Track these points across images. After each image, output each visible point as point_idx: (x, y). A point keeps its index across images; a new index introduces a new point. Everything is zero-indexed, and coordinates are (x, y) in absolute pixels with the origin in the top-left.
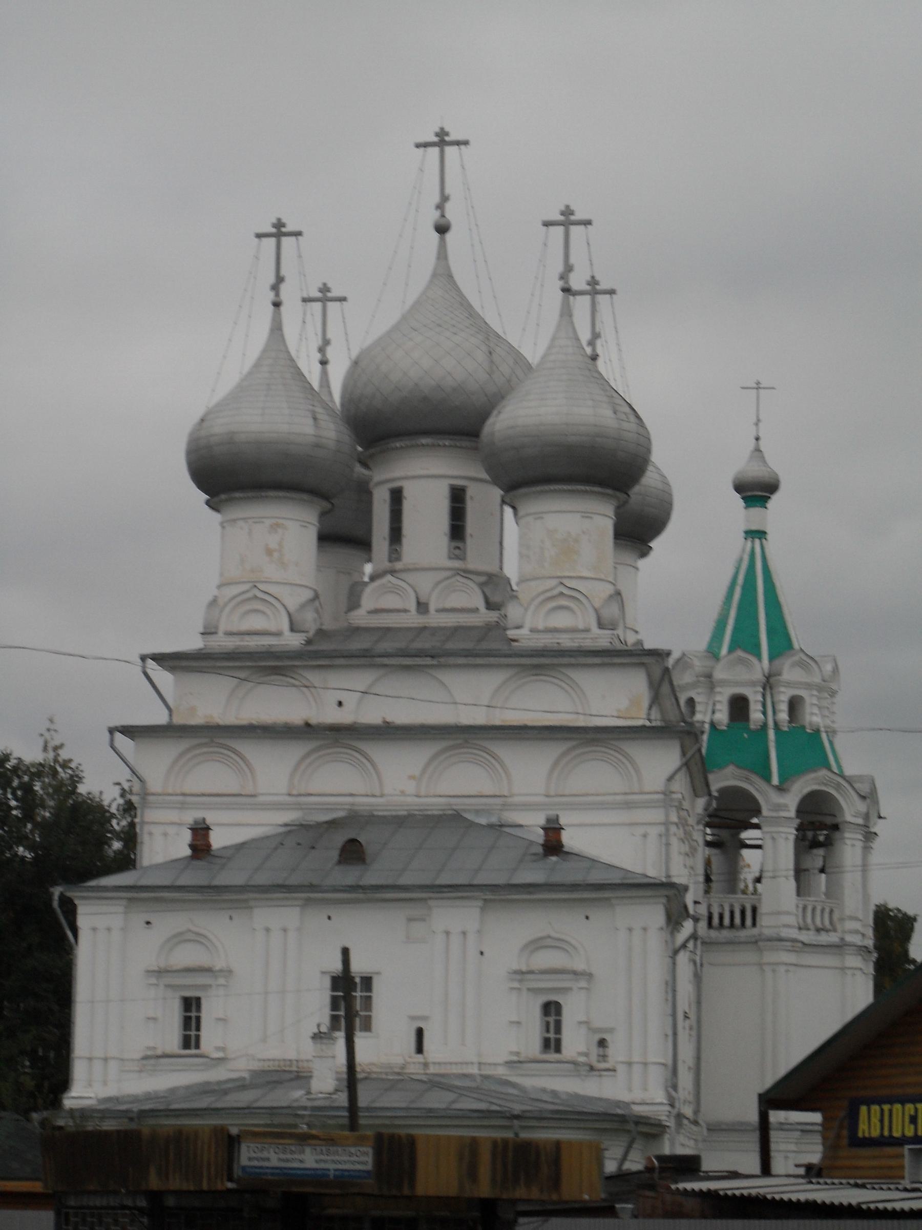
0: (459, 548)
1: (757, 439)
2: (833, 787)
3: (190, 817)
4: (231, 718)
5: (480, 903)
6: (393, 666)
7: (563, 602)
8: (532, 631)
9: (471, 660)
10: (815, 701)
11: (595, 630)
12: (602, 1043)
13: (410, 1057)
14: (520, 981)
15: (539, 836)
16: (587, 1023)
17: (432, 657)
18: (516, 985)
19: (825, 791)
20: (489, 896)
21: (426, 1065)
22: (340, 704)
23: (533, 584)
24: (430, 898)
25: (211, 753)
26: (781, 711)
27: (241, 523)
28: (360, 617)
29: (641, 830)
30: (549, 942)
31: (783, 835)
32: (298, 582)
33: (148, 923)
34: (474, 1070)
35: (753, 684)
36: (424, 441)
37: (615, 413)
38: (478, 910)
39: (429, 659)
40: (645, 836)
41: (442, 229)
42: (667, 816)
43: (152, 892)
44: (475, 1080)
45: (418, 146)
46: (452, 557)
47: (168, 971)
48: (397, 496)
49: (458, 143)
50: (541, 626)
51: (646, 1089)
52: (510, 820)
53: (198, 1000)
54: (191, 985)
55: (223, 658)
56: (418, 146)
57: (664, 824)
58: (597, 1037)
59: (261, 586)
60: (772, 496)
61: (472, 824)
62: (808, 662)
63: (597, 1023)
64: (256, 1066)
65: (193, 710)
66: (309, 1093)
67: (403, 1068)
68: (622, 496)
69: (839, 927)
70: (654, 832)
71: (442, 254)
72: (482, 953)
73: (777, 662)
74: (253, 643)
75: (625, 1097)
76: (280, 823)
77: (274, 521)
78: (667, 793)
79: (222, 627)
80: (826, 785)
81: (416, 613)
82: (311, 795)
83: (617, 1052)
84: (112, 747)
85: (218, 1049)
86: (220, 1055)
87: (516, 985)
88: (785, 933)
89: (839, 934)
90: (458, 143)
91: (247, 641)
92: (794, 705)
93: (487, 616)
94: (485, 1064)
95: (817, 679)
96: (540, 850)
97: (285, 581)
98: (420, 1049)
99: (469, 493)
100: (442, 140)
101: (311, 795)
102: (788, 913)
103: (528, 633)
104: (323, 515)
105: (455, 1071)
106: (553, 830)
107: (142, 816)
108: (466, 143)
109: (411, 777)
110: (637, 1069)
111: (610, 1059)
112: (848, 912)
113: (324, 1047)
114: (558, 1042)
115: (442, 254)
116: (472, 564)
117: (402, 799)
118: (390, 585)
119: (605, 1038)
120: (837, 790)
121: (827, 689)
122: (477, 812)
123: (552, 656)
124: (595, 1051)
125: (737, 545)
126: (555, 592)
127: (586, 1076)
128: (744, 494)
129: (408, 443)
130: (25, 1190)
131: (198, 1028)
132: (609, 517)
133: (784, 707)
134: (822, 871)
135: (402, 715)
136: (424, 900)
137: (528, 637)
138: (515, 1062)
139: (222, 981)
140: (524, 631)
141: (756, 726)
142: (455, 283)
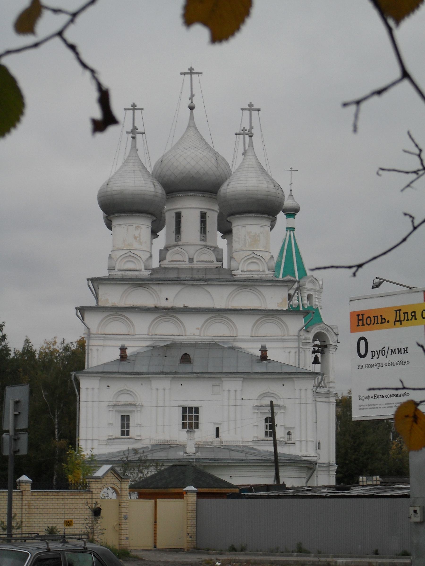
0: (204, 237)
1: (291, 191)
2: (325, 331)
3: (120, 343)
4: (122, 304)
5: (242, 379)
6: (188, 284)
11: (267, 271)
12: (289, 433)
13: (214, 439)
14: (258, 409)
15: (259, 354)
17: (205, 281)
18: (256, 411)
19: (325, 334)
20: (246, 377)
21: (221, 442)
22: (167, 299)
23: (241, 253)
25: (116, 318)
26: (304, 300)
27: (123, 226)
28: (165, 264)
29: (288, 350)
31: (308, 350)
32: (146, 250)
33: (108, 386)
34: (240, 444)
36: (191, 194)
37: (274, 186)
38: (241, 382)
39: (204, 282)
40: (289, 352)
41: (192, 108)
42: (299, 345)
43: (88, 374)
44: (241, 448)
45: (182, 74)
46: (202, 240)
47: (117, 405)
48: (178, 216)
49: (198, 73)
50: (245, 270)
51: (307, 451)
52: (236, 346)
54: (126, 411)
55: (119, 280)
56: (182, 74)
58: (287, 431)
60: (297, 214)
63: (288, 426)
64: (153, 442)
65: (107, 300)
66: (186, 453)
67: (212, 443)
68: (273, 218)
69: (327, 386)
70: (293, 351)
75: (299, 454)
76: (145, 346)
77: (137, 225)
78: (298, 336)
79: (117, 267)
80: (323, 330)
81: (188, 263)
82: (157, 335)
83: (295, 436)
84: (76, 315)
85: (138, 436)
86: (139, 438)
87: (256, 411)
89: (327, 389)
90: (198, 73)
91: (127, 273)
92: (309, 297)
93: (217, 264)
94: (244, 441)
96: (260, 358)
97: (142, 250)
98: (217, 435)
99: (207, 215)
100: (191, 72)
101: (157, 335)
103: (240, 272)
104: (153, 222)
105: (233, 444)
106: (264, 350)
107: (89, 343)
109: (198, 329)
110: (304, 443)
111: (292, 440)
112: (331, 380)
113: (191, 435)
116: (209, 243)
117: (194, 337)
118: (177, 251)
119: (290, 431)
120: (327, 332)
121: (320, 291)
122: (224, 342)
123: (253, 282)
124: (287, 436)
126: (251, 256)
127: (284, 446)
128: (286, 213)
129: (185, 194)
130: (206, 491)
132: (269, 226)
135: (191, 304)
136: (220, 378)
137: (240, 274)
139: (139, 409)
140: (239, 271)
141: (295, 306)
142: (198, 130)
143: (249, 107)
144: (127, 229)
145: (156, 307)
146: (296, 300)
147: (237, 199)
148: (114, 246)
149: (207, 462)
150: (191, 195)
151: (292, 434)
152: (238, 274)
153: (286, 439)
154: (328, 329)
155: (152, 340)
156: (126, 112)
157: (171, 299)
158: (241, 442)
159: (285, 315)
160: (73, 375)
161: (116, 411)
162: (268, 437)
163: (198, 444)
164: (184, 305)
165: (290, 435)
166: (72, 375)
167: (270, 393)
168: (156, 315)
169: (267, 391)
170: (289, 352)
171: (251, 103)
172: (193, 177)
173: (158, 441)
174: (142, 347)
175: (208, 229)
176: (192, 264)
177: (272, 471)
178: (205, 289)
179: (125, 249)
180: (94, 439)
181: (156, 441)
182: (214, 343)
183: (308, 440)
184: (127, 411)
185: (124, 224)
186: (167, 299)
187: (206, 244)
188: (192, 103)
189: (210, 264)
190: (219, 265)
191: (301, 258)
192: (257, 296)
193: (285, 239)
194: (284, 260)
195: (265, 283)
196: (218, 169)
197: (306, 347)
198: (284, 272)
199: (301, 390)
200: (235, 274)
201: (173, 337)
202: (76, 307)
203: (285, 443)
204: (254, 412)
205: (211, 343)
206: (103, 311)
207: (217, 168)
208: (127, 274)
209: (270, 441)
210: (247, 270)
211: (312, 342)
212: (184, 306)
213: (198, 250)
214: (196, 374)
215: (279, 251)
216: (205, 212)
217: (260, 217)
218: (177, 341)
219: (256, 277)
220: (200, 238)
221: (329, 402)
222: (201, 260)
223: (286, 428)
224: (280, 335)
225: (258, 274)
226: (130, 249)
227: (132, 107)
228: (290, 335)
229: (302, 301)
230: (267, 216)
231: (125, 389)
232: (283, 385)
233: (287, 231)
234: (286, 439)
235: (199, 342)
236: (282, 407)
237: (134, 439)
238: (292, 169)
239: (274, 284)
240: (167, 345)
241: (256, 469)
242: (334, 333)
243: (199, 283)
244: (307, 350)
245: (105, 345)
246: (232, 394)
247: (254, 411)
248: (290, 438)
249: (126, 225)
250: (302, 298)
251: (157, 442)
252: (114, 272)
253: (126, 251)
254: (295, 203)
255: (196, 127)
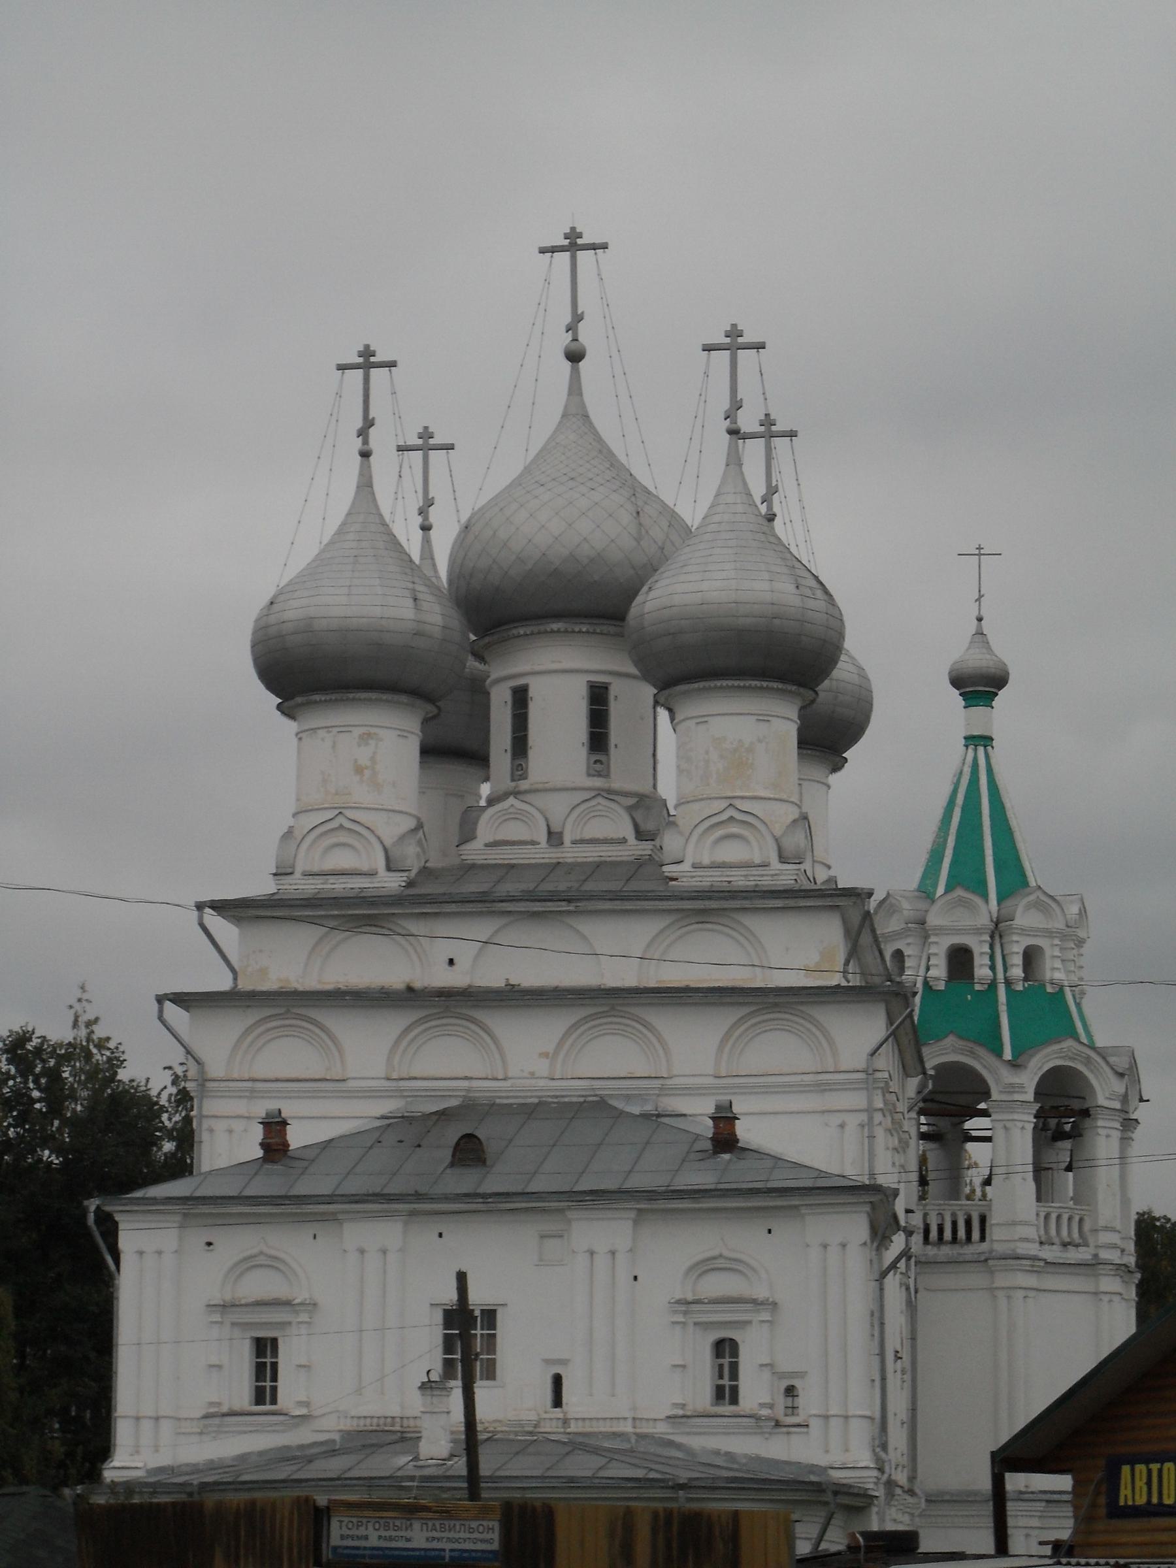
1: (980, 619)
2: (1081, 1062)
3: (261, 1108)
4: (311, 983)
5: (633, 1215)
7: (734, 829)
8: (694, 866)
9: (617, 905)
10: (1057, 953)
12: (790, 1391)
14: (685, 1313)
15: (706, 1128)
16: (770, 1366)
17: (569, 901)
21: (566, 1422)
22: (451, 962)
24: (569, 1208)
27: (321, 733)
28: (475, 851)
29: (836, 1120)
30: (720, 1263)
31: (1020, 1124)
33: (209, 1244)
34: (628, 1428)
35: (978, 931)
36: (555, 626)
38: (630, 1223)
39: (564, 903)
40: (842, 1126)
41: (575, 356)
42: (870, 1101)
44: (629, 1441)
45: (543, 251)
48: (521, 697)
49: (594, 247)
50: (706, 861)
53: (274, 1341)
54: (265, 1322)
56: (543, 251)
57: (866, 1110)
59: (348, 813)
61: (621, 1114)
62: (1047, 903)
63: (785, 1366)
64: (348, 1425)
65: (263, 971)
66: (416, 1459)
67: (536, 1426)
68: (809, 694)
69: (1091, 1241)
70: (853, 1121)
71: (575, 387)
72: (635, 1278)
73: (1008, 903)
74: (339, 886)
75: (821, 1460)
76: (378, 1115)
78: (870, 1071)
79: (299, 869)
80: (1071, 1059)
82: (415, 1078)
83: (809, 1402)
86: (304, 1411)
88: (1023, 1249)
89: (1092, 1250)
90: (594, 247)
92: (1031, 957)
93: (636, 849)
95: (1059, 924)
96: (708, 1145)
98: (558, 1402)
99: (613, 692)
100: (573, 244)
101: (415, 1078)
102: (1025, 1223)
104: (426, 722)
105: (603, 1429)
106: (724, 1120)
107: (200, 1108)
108: (604, 246)
109: (545, 1055)
112: (1102, 1223)
113: (435, 1400)
114: (735, 1391)
115: (575, 387)
117: (533, 1082)
118: (511, 810)
122: (628, 1098)
124: (781, 1401)
125: (954, 753)
126: (724, 817)
127: (770, 1433)
128: (962, 691)
129: (535, 629)
131: (274, 1378)
132: (791, 720)
133: (1018, 960)
134: (1069, 1168)
136: (560, 1211)
137: (689, 874)
138: (675, 1417)
139: (304, 1317)
140: (686, 866)
143: (728, 340)
144: (334, 743)
145: (410, 989)
146: (985, 965)
147: (673, 634)
148: (298, 800)
149: (455, 1489)
150: (556, 629)
151: (801, 1392)
152: (681, 874)
153: (779, 1412)
154: (1088, 1058)
155: (399, 1094)
156: (343, 373)
157: (463, 963)
158: (630, 1422)
159: (829, 1002)
160: (93, 1208)
161: (233, 1324)
162: (724, 1405)
163: (491, 1429)
164: (507, 979)
165: (793, 1396)
166: (85, 1212)
167: (726, 1258)
168: (414, 1015)
169: (716, 1253)
170: (842, 1126)
171: (734, 326)
172: (556, 570)
173: (362, 1422)
174: (370, 1117)
175: (614, 738)
176: (560, 850)
177: (815, 1519)
178: (578, 931)
179: (326, 806)
180: (141, 1414)
181: (355, 1422)
182: (596, 1101)
183: (850, 1413)
184: (271, 1323)
185: (326, 727)
186: (451, 962)
187: (606, 786)
188: (575, 340)
189: (604, 849)
190: (644, 850)
191: (1009, 831)
192: (737, 941)
193: (961, 773)
194: (954, 838)
195: (761, 901)
196: (642, 543)
197: (1011, 1117)
198: (951, 876)
199: (829, 1248)
200: (674, 875)
201: (465, 1084)
202: (157, 995)
203: (773, 1424)
204: (673, 1323)
205: (588, 1102)
206: (248, 1006)
207: (638, 540)
208: (333, 886)
209: (725, 1416)
210: (712, 863)
211: (1032, 1100)
212: (506, 985)
213: (578, 805)
214: (481, 1200)
215: (942, 811)
216: (604, 683)
217: (750, 687)
218: (479, 1097)
219: (740, 883)
220: (588, 768)
221: (1096, 1294)
222: (587, 836)
223: (782, 1376)
224: (814, 1070)
225: (745, 873)
226: (343, 805)
227: (361, 360)
228: (842, 1069)
229: (1005, 970)
230: (775, 685)
231: (261, 1253)
232: (770, 1231)
233: (967, 746)
234: (779, 1412)
235: (550, 1100)
236: (762, 1303)
237: (286, 1414)
238: (982, 552)
239: (791, 903)
240: (445, 1109)
241: (1056, 1509)
242: (1113, 1069)
243: (551, 906)
244: (1015, 1125)
245: (252, 1115)
246: (601, 1261)
247: (672, 1320)
248: (793, 1408)
249: (329, 732)
250: (1007, 958)
251: (362, 1425)
252: (291, 882)
253: (329, 815)
254: (988, 657)
255: (586, 416)
